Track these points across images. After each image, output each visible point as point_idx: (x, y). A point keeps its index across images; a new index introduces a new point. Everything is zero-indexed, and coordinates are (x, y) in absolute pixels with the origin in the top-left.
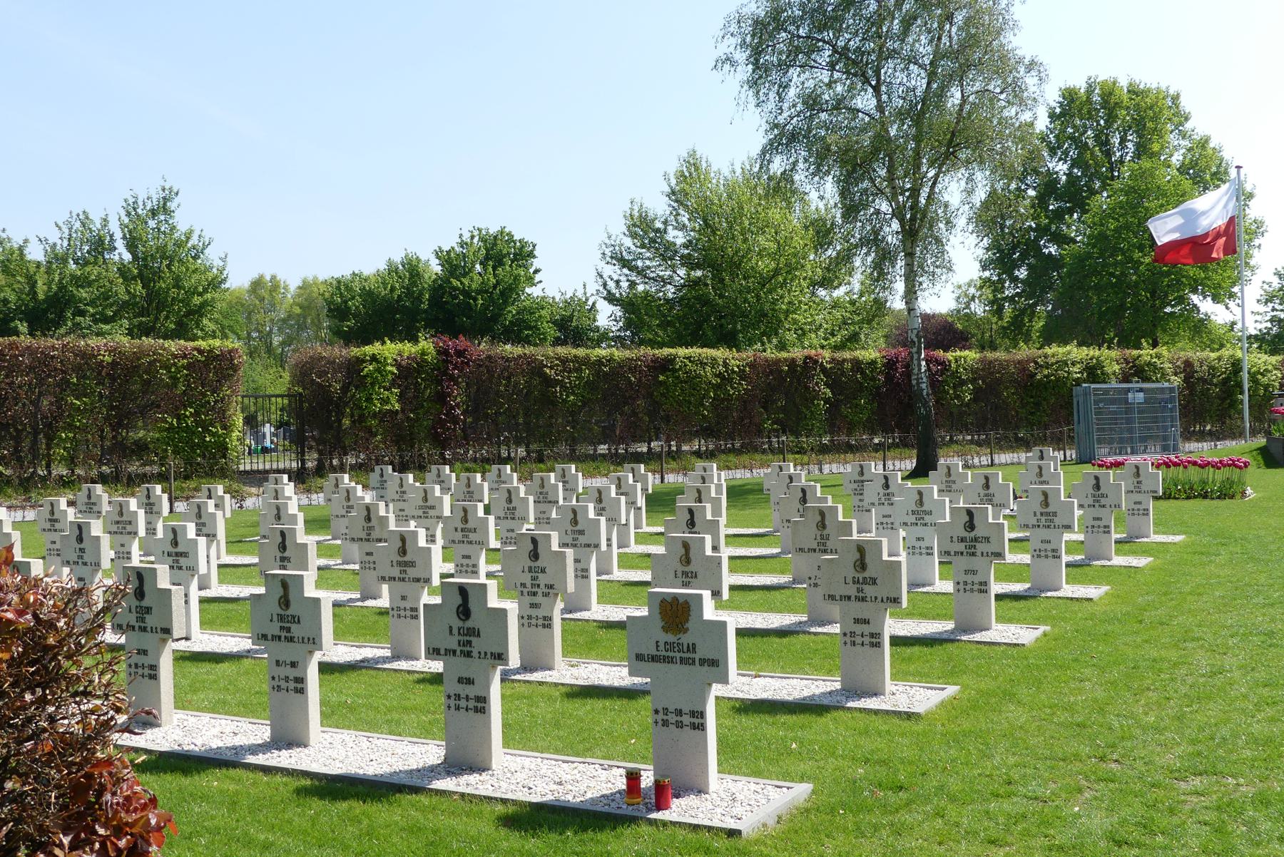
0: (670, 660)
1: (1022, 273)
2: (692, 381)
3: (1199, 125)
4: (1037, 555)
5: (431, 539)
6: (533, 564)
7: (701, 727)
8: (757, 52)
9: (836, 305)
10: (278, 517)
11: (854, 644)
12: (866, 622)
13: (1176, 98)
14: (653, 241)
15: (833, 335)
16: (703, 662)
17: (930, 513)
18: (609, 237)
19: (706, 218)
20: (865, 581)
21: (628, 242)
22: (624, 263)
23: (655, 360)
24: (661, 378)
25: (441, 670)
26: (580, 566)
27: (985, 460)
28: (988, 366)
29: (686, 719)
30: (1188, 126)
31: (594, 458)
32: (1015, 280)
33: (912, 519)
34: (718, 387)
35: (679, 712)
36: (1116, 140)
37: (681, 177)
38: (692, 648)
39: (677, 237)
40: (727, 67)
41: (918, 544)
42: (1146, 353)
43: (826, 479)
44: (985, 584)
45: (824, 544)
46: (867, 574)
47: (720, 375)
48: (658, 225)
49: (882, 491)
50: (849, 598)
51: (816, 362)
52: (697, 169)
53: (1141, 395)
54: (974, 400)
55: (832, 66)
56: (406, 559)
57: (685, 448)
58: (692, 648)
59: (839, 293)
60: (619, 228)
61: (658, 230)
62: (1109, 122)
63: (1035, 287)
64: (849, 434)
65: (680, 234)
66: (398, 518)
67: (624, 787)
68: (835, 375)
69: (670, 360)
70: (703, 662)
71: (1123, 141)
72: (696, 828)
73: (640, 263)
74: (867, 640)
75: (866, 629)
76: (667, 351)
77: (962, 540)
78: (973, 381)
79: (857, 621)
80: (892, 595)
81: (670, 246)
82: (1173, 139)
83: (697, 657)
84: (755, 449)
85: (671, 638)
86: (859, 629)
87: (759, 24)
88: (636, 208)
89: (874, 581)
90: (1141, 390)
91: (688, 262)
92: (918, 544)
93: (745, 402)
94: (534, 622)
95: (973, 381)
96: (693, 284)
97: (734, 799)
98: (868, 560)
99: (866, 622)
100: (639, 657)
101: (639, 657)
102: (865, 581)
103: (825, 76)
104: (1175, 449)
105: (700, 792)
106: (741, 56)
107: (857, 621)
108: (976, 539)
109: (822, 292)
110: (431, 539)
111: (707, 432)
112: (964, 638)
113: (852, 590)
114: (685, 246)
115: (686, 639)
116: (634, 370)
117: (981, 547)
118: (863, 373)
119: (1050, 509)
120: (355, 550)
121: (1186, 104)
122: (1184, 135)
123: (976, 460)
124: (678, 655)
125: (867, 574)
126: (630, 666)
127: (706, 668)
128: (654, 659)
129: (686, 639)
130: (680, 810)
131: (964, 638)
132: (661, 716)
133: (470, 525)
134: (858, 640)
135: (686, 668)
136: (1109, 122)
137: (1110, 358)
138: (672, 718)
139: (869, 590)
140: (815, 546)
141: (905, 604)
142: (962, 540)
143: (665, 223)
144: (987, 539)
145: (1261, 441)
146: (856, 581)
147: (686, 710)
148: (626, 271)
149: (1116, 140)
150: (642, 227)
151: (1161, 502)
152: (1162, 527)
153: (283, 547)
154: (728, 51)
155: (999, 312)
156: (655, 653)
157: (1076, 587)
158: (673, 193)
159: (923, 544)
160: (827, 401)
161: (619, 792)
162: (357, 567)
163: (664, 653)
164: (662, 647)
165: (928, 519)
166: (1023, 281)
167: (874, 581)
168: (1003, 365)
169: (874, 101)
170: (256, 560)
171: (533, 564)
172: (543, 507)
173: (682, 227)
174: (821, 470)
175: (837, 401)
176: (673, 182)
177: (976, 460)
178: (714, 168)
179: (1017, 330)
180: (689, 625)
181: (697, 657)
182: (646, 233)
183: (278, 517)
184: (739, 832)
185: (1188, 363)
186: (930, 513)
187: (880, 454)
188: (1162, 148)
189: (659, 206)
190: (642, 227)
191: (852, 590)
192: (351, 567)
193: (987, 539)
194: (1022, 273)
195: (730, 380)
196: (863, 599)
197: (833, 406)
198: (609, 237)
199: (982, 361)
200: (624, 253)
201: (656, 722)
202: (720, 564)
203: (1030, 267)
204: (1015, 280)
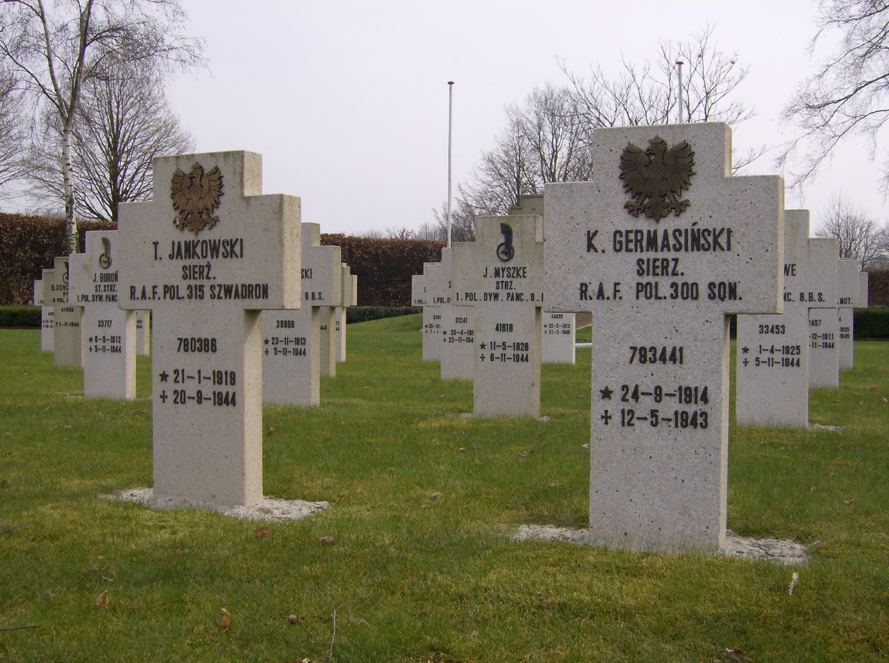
17: (231, 249)
186: (231, 249)
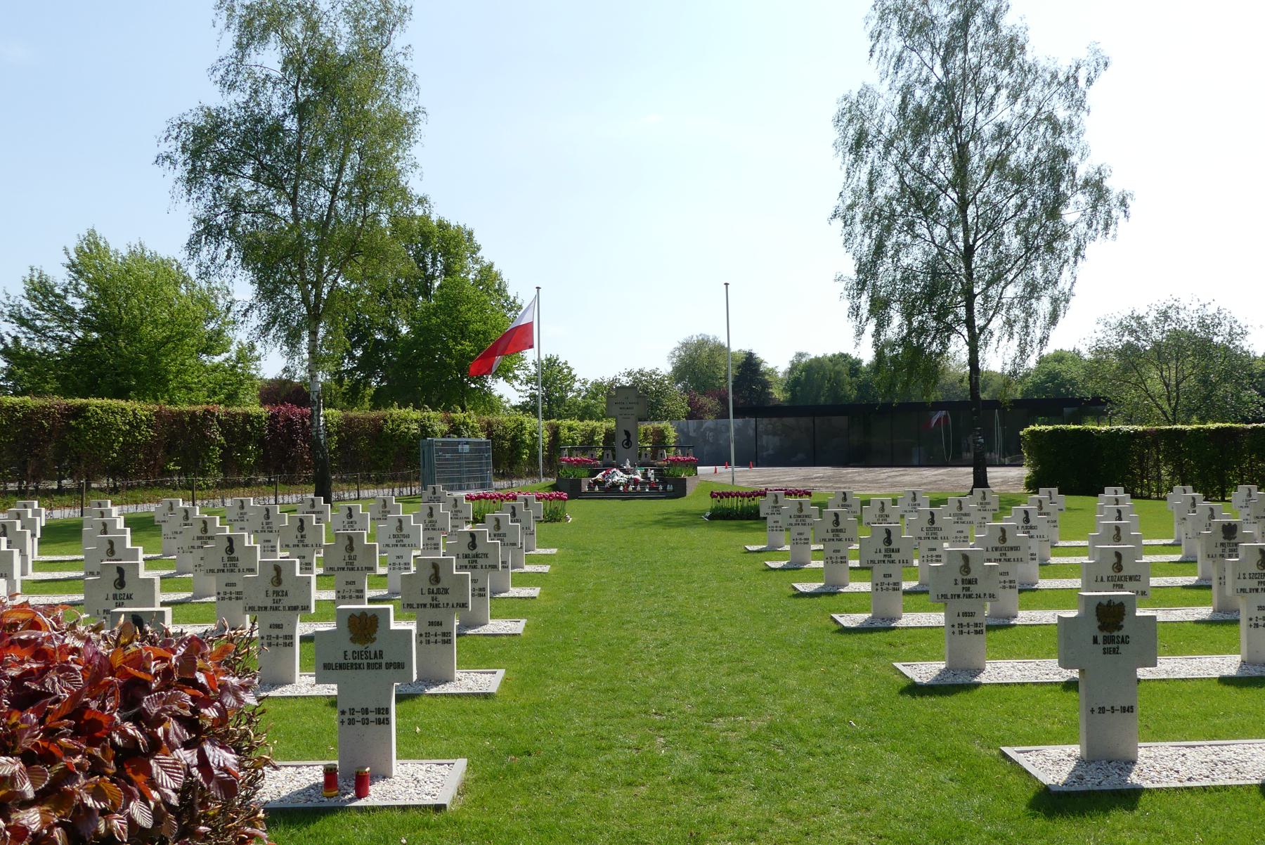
0: (358, 667)
1: (359, 353)
2: (105, 428)
3: (486, 255)
4: (828, 560)
5: (307, 567)
6: (118, 592)
7: (387, 722)
8: (196, 155)
9: (215, 368)
10: (111, 552)
11: (428, 642)
12: (439, 624)
13: (470, 234)
14: (52, 304)
15: (215, 393)
16: (389, 666)
17: (408, 536)
18: (8, 298)
19: (103, 290)
20: (438, 591)
21: (26, 303)
22: (22, 322)
23: (68, 408)
24: (73, 423)
25: (335, 693)
26: (477, 586)
27: (353, 495)
28: (349, 422)
29: (372, 716)
30: (479, 254)
31: (61, 491)
32: (352, 357)
33: (393, 541)
34: (129, 432)
35: (366, 711)
36: (429, 261)
37: (80, 251)
38: (380, 654)
39: (79, 305)
40: (167, 163)
41: (397, 561)
42: (459, 416)
43: (220, 512)
44: (362, 591)
45: (352, 564)
46: (440, 586)
47: (130, 423)
48: (57, 291)
49: (346, 520)
50: (425, 605)
51: (213, 414)
52: (97, 245)
53: (467, 447)
54: (338, 449)
55: (256, 178)
56: (969, 577)
57: (94, 485)
58: (380, 654)
59: (217, 360)
60: (18, 291)
61: (57, 296)
62: (425, 245)
63: (368, 364)
64: (239, 474)
65: (78, 300)
66: (264, 550)
67: (322, 780)
68: (227, 426)
69: (82, 409)
70: (389, 666)
71: (434, 259)
72: (404, 808)
73: (38, 323)
74: (439, 638)
75: (439, 630)
76: (79, 401)
77: (466, 556)
78: (338, 433)
79: (431, 624)
80: (462, 601)
81: (69, 310)
82: (469, 262)
83: (383, 662)
84: (162, 485)
85: (358, 647)
86: (433, 630)
87: (198, 132)
88: (36, 274)
89: (446, 591)
90: (467, 443)
91: (86, 325)
92: (397, 561)
93: (149, 447)
94: (965, 629)
95: (338, 433)
96: (82, 344)
97: (417, 780)
98: (441, 574)
99: (439, 624)
100: (327, 666)
101: (327, 666)
102: (438, 591)
103: (248, 186)
104: (490, 486)
105: (384, 778)
106: (180, 157)
107: (431, 624)
108: (477, 556)
109: (204, 357)
110: (307, 567)
111: (115, 471)
112: (470, 632)
113: (427, 599)
114: (84, 311)
115: (373, 647)
116: (47, 416)
117: (481, 561)
118: (252, 426)
119: (501, 531)
120: (212, 583)
121: (478, 238)
122: (476, 262)
123: (346, 495)
124: (365, 662)
125: (440, 586)
126: (316, 676)
127: (392, 670)
128: (341, 667)
129: (373, 647)
130: (377, 795)
131: (470, 632)
132: (347, 716)
133: (479, 550)
134: (432, 639)
135: (373, 672)
136: (425, 245)
137: (436, 420)
138: (358, 717)
139: (442, 599)
140: (343, 565)
141: (313, 611)
142: (466, 556)
143: (66, 290)
144: (486, 555)
145: (553, 481)
146: (431, 592)
147: (372, 707)
148: (24, 329)
149: (429, 261)
150: (41, 290)
151: (543, 524)
152: (545, 543)
153: (120, 583)
154: (169, 150)
155: (340, 381)
156: (342, 661)
157: (518, 589)
158: (74, 265)
159: (402, 561)
160: (222, 446)
161: (316, 785)
162: (213, 599)
163: (352, 661)
164: (350, 654)
165: (842, 535)
166: (358, 359)
167: (446, 591)
168: (360, 422)
169: (289, 209)
170: (81, 597)
171: (118, 592)
172: (431, 534)
173: (80, 295)
174: (223, 502)
175: (230, 447)
176: (74, 256)
177: (346, 495)
178: (112, 248)
179: (353, 396)
180: (378, 635)
181: (383, 662)
182: (46, 297)
183: (111, 552)
184: (445, 806)
185: (489, 424)
186: (408, 536)
187: (272, 489)
188: (462, 268)
189: (59, 276)
190: (41, 290)
191: (427, 599)
192: (208, 599)
193: (486, 555)
194: (359, 353)
195: (138, 427)
196: (437, 606)
197: (226, 452)
198: (8, 298)
199: (346, 418)
200: (23, 313)
201: (342, 722)
202: (309, 583)
203: (365, 349)
204: (352, 357)
